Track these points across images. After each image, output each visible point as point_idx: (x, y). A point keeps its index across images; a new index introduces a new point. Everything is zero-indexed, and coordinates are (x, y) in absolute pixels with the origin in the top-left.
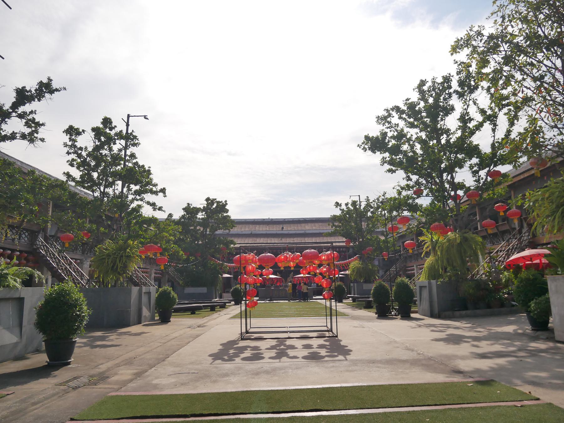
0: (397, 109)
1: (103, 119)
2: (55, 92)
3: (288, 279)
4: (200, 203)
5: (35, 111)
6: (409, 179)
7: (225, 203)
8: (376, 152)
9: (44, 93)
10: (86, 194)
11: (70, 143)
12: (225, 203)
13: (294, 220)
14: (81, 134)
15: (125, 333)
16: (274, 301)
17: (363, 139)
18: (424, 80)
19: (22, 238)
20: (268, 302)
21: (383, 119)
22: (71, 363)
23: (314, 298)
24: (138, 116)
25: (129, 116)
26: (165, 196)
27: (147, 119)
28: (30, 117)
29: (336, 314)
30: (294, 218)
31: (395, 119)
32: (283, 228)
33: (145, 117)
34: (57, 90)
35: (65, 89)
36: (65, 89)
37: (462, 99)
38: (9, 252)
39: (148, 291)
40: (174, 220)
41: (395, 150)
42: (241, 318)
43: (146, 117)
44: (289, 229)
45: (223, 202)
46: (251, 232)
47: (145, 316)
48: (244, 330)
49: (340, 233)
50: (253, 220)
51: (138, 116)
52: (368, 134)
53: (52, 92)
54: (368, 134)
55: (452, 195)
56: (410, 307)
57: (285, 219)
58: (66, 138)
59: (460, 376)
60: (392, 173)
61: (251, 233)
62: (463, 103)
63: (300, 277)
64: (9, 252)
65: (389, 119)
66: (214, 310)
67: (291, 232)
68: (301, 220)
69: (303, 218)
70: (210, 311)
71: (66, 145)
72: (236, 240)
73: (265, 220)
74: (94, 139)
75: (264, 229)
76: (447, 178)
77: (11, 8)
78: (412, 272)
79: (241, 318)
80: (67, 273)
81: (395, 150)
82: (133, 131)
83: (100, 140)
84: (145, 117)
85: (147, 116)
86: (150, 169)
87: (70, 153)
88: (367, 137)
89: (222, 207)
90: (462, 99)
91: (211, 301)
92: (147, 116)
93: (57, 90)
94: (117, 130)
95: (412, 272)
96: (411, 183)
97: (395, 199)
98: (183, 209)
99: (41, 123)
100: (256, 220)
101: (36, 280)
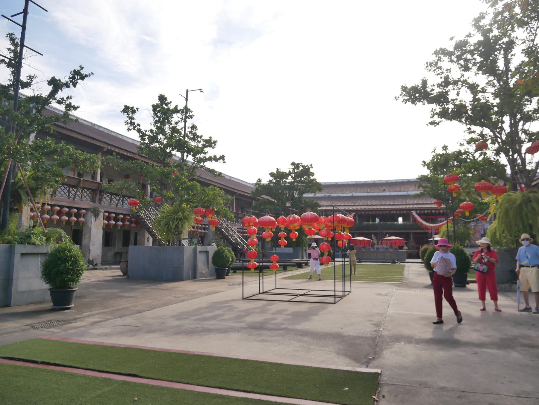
0: (444, 52)
2: (86, 78)
4: (286, 168)
5: (71, 96)
6: (471, 132)
8: (416, 104)
9: (77, 80)
11: (129, 121)
14: (135, 112)
16: (363, 263)
18: (485, 12)
19: (124, 204)
20: (390, 264)
21: (434, 65)
22: (72, 308)
25: (187, 91)
26: (224, 163)
27: (202, 92)
28: (68, 102)
29: (335, 277)
31: (445, 63)
33: (201, 91)
34: (86, 76)
35: (93, 74)
36: (93, 74)
37: (527, 29)
38: (114, 215)
39: (206, 250)
40: (263, 185)
41: (441, 99)
42: (335, 280)
43: (202, 90)
47: (201, 273)
49: (430, 194)
53: (83, 77)
56: (466, 277)
57: (387, 181)
58: (125, 118)
59: (123, 345)
60: (435, 126)
61: (352, 196)
62: (528, 33)
64: (114, 215)
65: (439, 65)
66: (286, 270)
68: (405, 181)
69: (407, 180)
71: (127, 123)
72: (322, 203)
73: (367, 182)
74: (153, 116)
76: (523, 128)
77: (47, 11)
79: (335, 280)
81: (441, 99)
83: (157, 116)
84: (201, 91)
87: (130, 130)
89: (306, 171)
90: (527, 29)
91: (291, 260)
93: (86, 76)
96: (474, 136)
97: (441, 155)
98: (270, 174)
99: (76, 106)
100: (358, 183)
101: (63, 239)
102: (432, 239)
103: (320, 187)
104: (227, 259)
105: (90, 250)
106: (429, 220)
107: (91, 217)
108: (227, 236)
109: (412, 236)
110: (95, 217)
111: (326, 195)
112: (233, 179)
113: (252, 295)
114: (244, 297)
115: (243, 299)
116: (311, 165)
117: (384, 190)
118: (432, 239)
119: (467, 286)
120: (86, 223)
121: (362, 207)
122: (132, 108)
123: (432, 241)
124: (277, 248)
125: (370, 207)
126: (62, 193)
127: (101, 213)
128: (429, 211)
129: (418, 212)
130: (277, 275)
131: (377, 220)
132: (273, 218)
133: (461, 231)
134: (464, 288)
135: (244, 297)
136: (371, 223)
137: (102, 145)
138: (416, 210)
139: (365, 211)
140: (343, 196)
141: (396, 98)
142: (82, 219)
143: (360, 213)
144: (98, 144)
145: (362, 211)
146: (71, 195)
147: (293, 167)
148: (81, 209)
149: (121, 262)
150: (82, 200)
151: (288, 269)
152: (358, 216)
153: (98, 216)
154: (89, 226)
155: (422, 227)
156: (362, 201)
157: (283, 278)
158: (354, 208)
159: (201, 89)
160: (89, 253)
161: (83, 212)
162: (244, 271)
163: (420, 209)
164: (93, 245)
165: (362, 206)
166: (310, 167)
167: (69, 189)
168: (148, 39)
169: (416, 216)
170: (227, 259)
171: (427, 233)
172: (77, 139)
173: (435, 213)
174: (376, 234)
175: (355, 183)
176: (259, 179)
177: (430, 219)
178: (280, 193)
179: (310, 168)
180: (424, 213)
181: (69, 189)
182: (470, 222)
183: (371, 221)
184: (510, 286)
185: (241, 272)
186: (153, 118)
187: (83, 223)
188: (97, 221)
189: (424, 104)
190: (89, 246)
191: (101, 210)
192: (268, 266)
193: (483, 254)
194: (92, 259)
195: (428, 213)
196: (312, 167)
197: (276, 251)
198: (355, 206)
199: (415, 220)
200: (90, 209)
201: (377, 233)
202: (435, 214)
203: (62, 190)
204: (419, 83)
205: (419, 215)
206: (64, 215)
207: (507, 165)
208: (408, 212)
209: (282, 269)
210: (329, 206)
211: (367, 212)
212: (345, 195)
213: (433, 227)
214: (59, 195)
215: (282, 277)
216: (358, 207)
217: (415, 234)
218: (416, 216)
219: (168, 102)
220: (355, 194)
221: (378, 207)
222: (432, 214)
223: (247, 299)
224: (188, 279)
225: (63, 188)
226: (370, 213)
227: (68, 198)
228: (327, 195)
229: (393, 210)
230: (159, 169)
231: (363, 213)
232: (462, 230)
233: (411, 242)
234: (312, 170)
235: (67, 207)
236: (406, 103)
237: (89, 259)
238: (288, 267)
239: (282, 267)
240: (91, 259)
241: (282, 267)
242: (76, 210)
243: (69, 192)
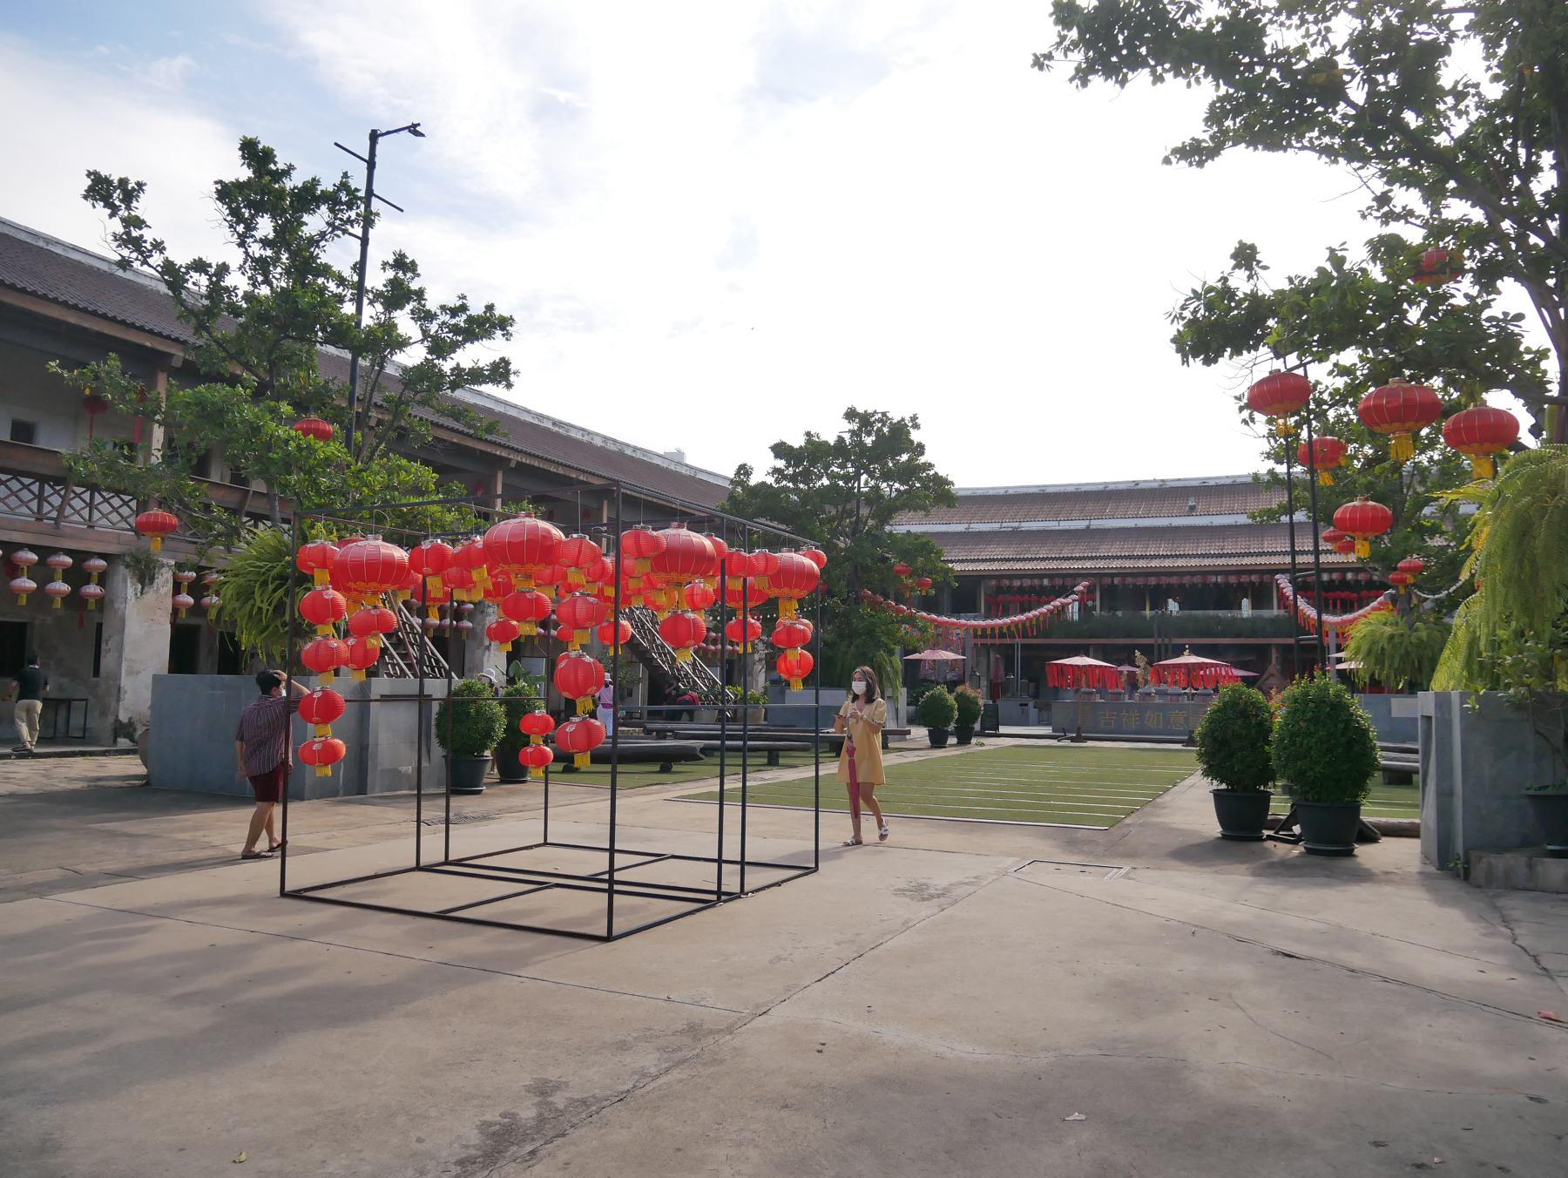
1: (240, 149)
10: (559, 427)
13: (1239, 480)
15: (113, 834)
16: (1090, 743)
20: (1179, 746)
25: (374, 137)
30: (1239, 477)
33: (413, 129)
42: (447, 822)
50: (1101, 488)
55: (1502, 224)
57: (1204, 480)
61: (1088, 527)
63: (1180, 665)
70: (660, 772)
73: (1141, 486)
78: (1018, 654)
79: (447, 822)
80: (645, 633)
85: (419, 125)
92: (419, 125)
94: (1357, 360)
95: (1018, 654)
100: (1111, 487)
103: (938, 493)
104: (481, 725)
105: (119, 688)
106: (1335, 606)
107: (125, 581)
108: (646, 651)
109: (1274, 655)
110: (142, 580)
111: (1004, 525)
112: (705, 477)
113: (373, 873)
114: (288, 888)
115: (284, 894)
116: (914, 418)
117: (1192, 508)
119: (1363, 851)
120: (112, 602)
121: (1115, 564)
122: (123, 182)
124: (820, 692)
125: (1141, 564)
126: (115, 517)
127: (164, 570)
128: (1335, 576)
130: (291, 806)
131: (1173, 606)
133: (1420, 639)
134: (1345, 863)
135: (288, 888)
136: (1148, 613)
137: (163, 347)
139: (1124, 574)
140: (1057, 528)
142: (93, 589)
144: (148, 344)
145: (1112, 576)
146: (46, 508)
147: (855, 426)
148: (91, 555)
149: (1273, 713)
150: (93, 527)
151: (781, 761)
152: (1101, 590)
153: (152, 580)
154: (120, 613)
156: (1117, 545)
157: (682, 797)
158: (1088, 564)
160: (118, 700)
161: (97, 568)
162: (620, 768)
164: (133, 673)
165: (1112, 559)
166: (910, 424)
167: (41, 489)
168: (562, 96)
170: (481, 725)
172: (58, 323)
173: (1357, 581)
174: (1147, 650)
176: (742, 467)
177: (1339, 602)
179: (911, 430)
181: (41, 489)
183: (1148, 608)
184: (1530, 867)
185: (608, 768)
186: (231, 226)
187: (101, 602)
188: (150, 596)
189: (1158, 79)
190: (117, 677)
191: (165, 561)
192: (693, 749)
194: (130, 719)
195: (1331, 581)
196: (916, 426)
197: (385, 699)
198: (1092, 558)
200: (124, 555)
201: (1152, 645)
202: (1355, 586)
203: (115, 510)
206: (23, 575)
207: (1549, 350)
208: (1266, 577)
209: (765, 761)
210: (1008, 560)
211: (1130, 580)
212: (1065, 525)
214: (104, 522)
215: (686, 793)
216: (1101, 564)
219: (281, 166)
220: (1096, 524)
221: (1167, 563)
222: (1344, 584)
223: (297, 895)
224: (327, 792)
225: (116, 502)
226: (1140, 581)
227: (37, 519)
228: (1009, 525)
229: (1217, 573)
231: (1116, 581)
232: (1424, 634)
233: (1272, 675)
234: (915, 436)
235: (32, 548)
236: (1085, 83)
237: (117, 720)
238: (781, 753)
239: (766, 753)
240: (123, 717)
241: (766, 753)
242: (69, 560)
243: (41, 498)
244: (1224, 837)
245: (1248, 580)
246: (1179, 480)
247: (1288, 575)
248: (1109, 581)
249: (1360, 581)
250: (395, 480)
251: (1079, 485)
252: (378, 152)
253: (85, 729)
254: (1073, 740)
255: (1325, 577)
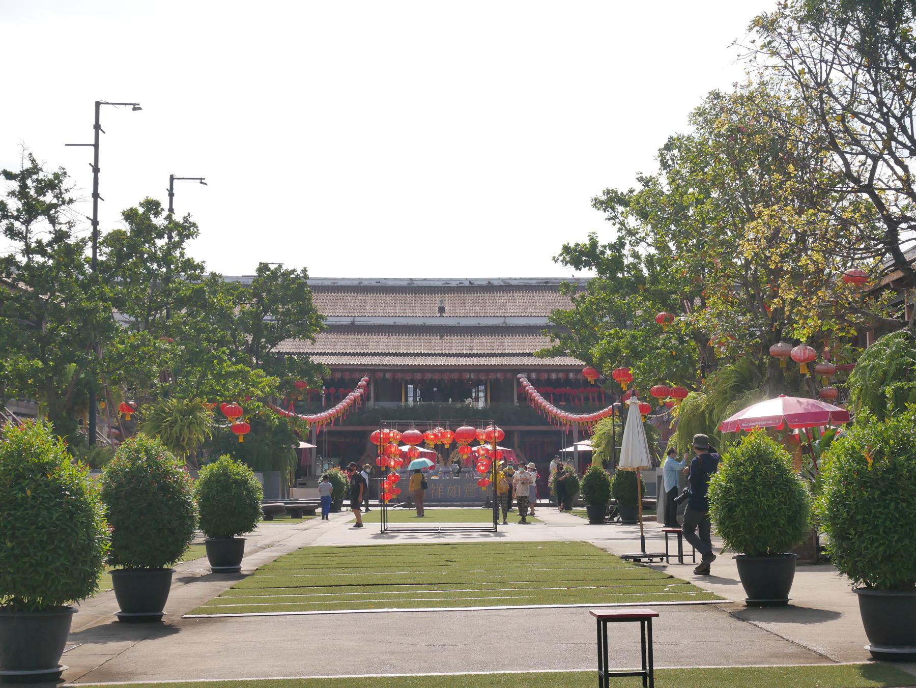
3: (451, 456)
7: (302, 275)
12: (302, 275)
17: (560, 250)
20: (401, 508)
23: (538, 501)
24: (113, 104)
25: (172, 178)
32: (441, 310)
33: (202, 181)
43: (203, 181)
44: (460, 312)
45: (299, 271)
46: (351, 319)
48: (383, 529)
51: (113, 104)
52: (568, 244)
54: (568, 244)
61: (353, 323)
67: (464, 322)
69: (503, 280)
75: (389, 311)
82: (189, 214)
84: (202, 181)
85: (204, 179)
86: (204, 264)
88: (566, 249)
92: (204, 179)
100: (365, 283)
102: (571, 449)
118: (571, 449)
123: (571, 453)
125: (408, 361)
128: (561, 375)
129: (534, 376)
132: (416, 431)
138: (527, 370)
139: (394, 369)
141: (554, 258)
143: (381, 375)
145: (385, 371)
155: (543, 417)
159: (201, 179)
163: (539, 369)
169: (530, 389)
171: (558, 433)
173: (577, 380)
175: (356, 283)
178: (253, 340)
180: (549, 380)
182: (788, 69)
193: (864, 535)
195: (558, 379)
199: (524, 396)
204: (586, 241)
205: (534, 383)
208: (509, 375)
213: (575, 420)
217: (524, 434)
218: (530, 389)
222: (567, 382)
230: (808, 521)
231: (388, 376)
244: (123, 619)
245: (494, 377)
246: (425, 279)
247: (526, 374)
248: (546, 376)
249: (579, 380)
250: (890, 565)
251: (335, 279)
252: (174, 187)
253: (667, 538)
254: (404, 506)
255: (554, 376)
